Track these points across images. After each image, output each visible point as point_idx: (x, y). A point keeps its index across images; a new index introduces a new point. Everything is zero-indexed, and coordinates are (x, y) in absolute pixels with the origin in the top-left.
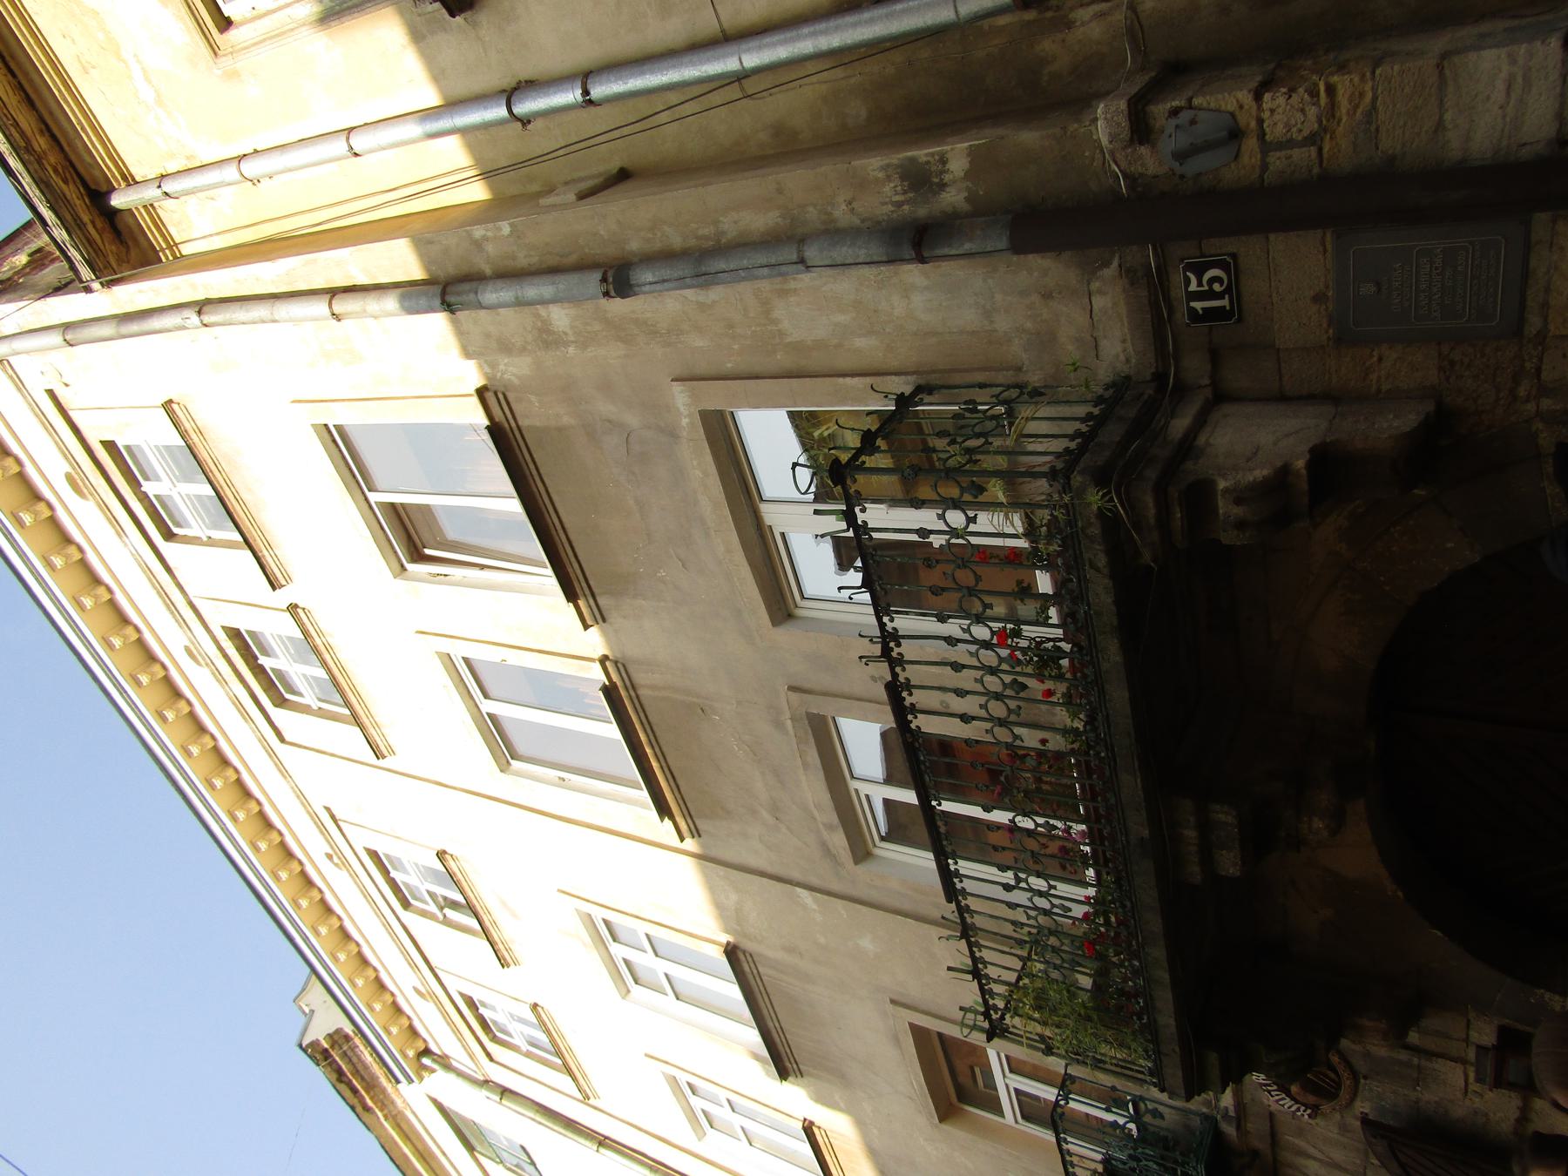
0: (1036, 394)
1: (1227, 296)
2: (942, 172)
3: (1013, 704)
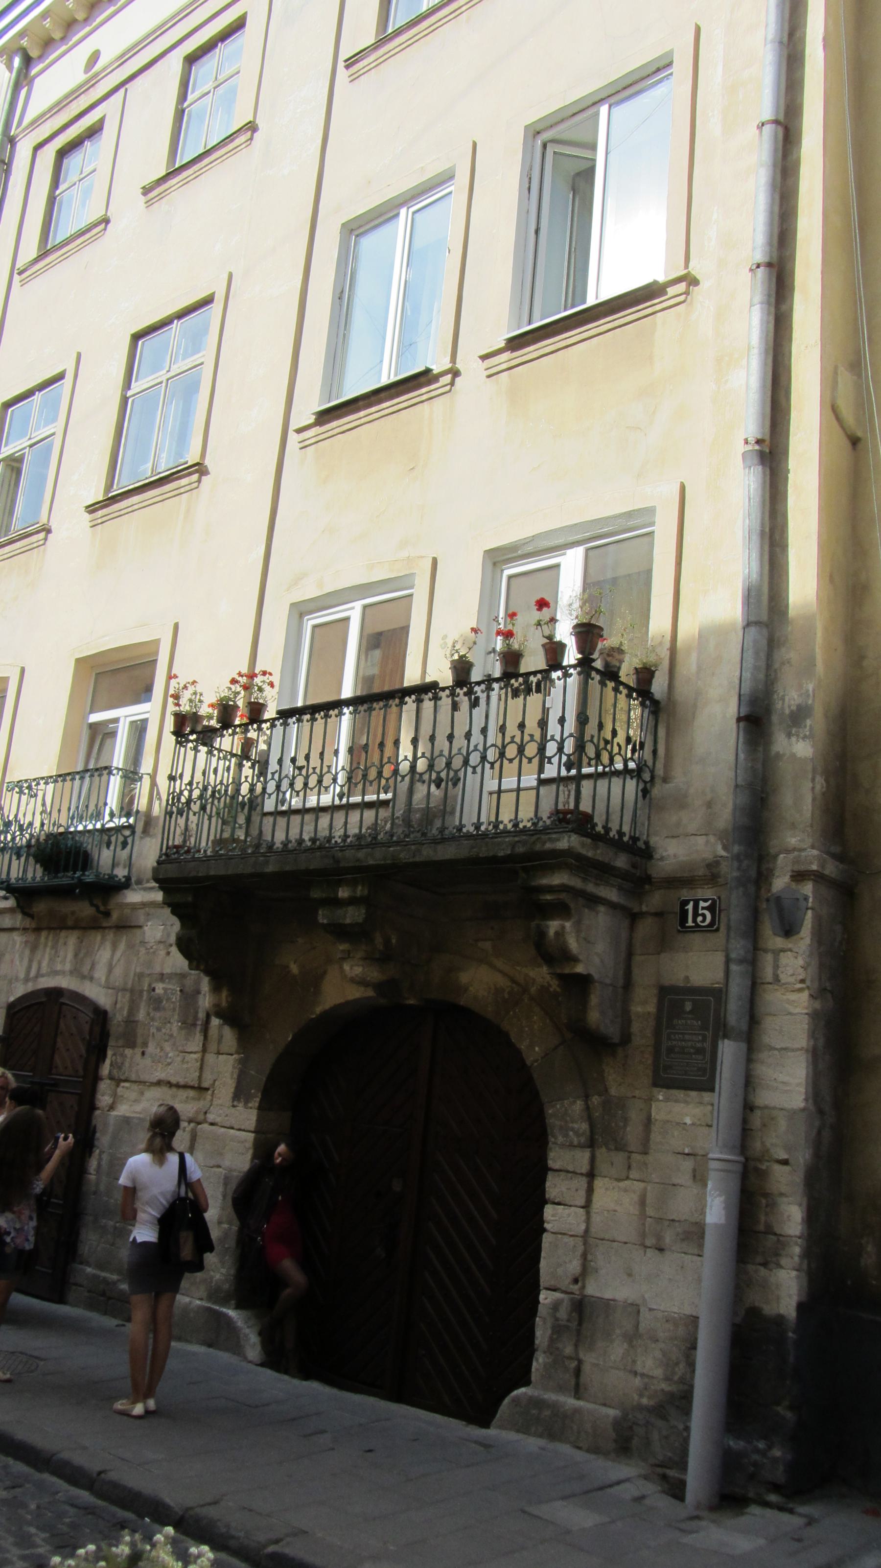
0: (645, 792)
1: (694, 924)
2: (798, 736)
3: (426, 777)
